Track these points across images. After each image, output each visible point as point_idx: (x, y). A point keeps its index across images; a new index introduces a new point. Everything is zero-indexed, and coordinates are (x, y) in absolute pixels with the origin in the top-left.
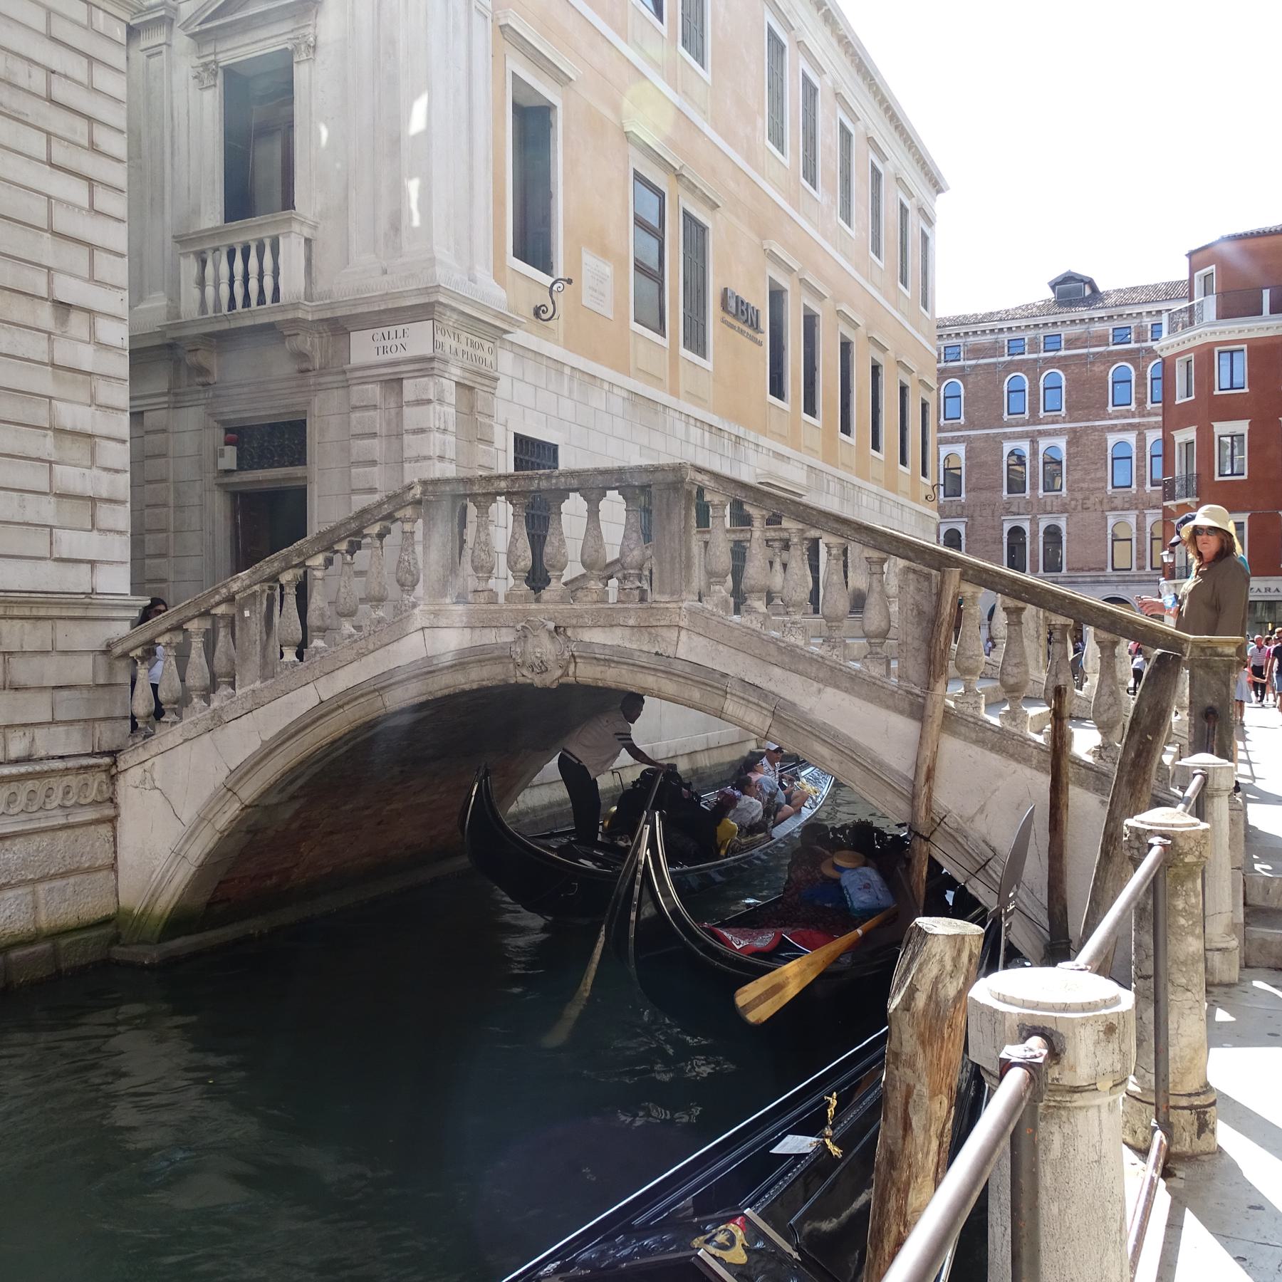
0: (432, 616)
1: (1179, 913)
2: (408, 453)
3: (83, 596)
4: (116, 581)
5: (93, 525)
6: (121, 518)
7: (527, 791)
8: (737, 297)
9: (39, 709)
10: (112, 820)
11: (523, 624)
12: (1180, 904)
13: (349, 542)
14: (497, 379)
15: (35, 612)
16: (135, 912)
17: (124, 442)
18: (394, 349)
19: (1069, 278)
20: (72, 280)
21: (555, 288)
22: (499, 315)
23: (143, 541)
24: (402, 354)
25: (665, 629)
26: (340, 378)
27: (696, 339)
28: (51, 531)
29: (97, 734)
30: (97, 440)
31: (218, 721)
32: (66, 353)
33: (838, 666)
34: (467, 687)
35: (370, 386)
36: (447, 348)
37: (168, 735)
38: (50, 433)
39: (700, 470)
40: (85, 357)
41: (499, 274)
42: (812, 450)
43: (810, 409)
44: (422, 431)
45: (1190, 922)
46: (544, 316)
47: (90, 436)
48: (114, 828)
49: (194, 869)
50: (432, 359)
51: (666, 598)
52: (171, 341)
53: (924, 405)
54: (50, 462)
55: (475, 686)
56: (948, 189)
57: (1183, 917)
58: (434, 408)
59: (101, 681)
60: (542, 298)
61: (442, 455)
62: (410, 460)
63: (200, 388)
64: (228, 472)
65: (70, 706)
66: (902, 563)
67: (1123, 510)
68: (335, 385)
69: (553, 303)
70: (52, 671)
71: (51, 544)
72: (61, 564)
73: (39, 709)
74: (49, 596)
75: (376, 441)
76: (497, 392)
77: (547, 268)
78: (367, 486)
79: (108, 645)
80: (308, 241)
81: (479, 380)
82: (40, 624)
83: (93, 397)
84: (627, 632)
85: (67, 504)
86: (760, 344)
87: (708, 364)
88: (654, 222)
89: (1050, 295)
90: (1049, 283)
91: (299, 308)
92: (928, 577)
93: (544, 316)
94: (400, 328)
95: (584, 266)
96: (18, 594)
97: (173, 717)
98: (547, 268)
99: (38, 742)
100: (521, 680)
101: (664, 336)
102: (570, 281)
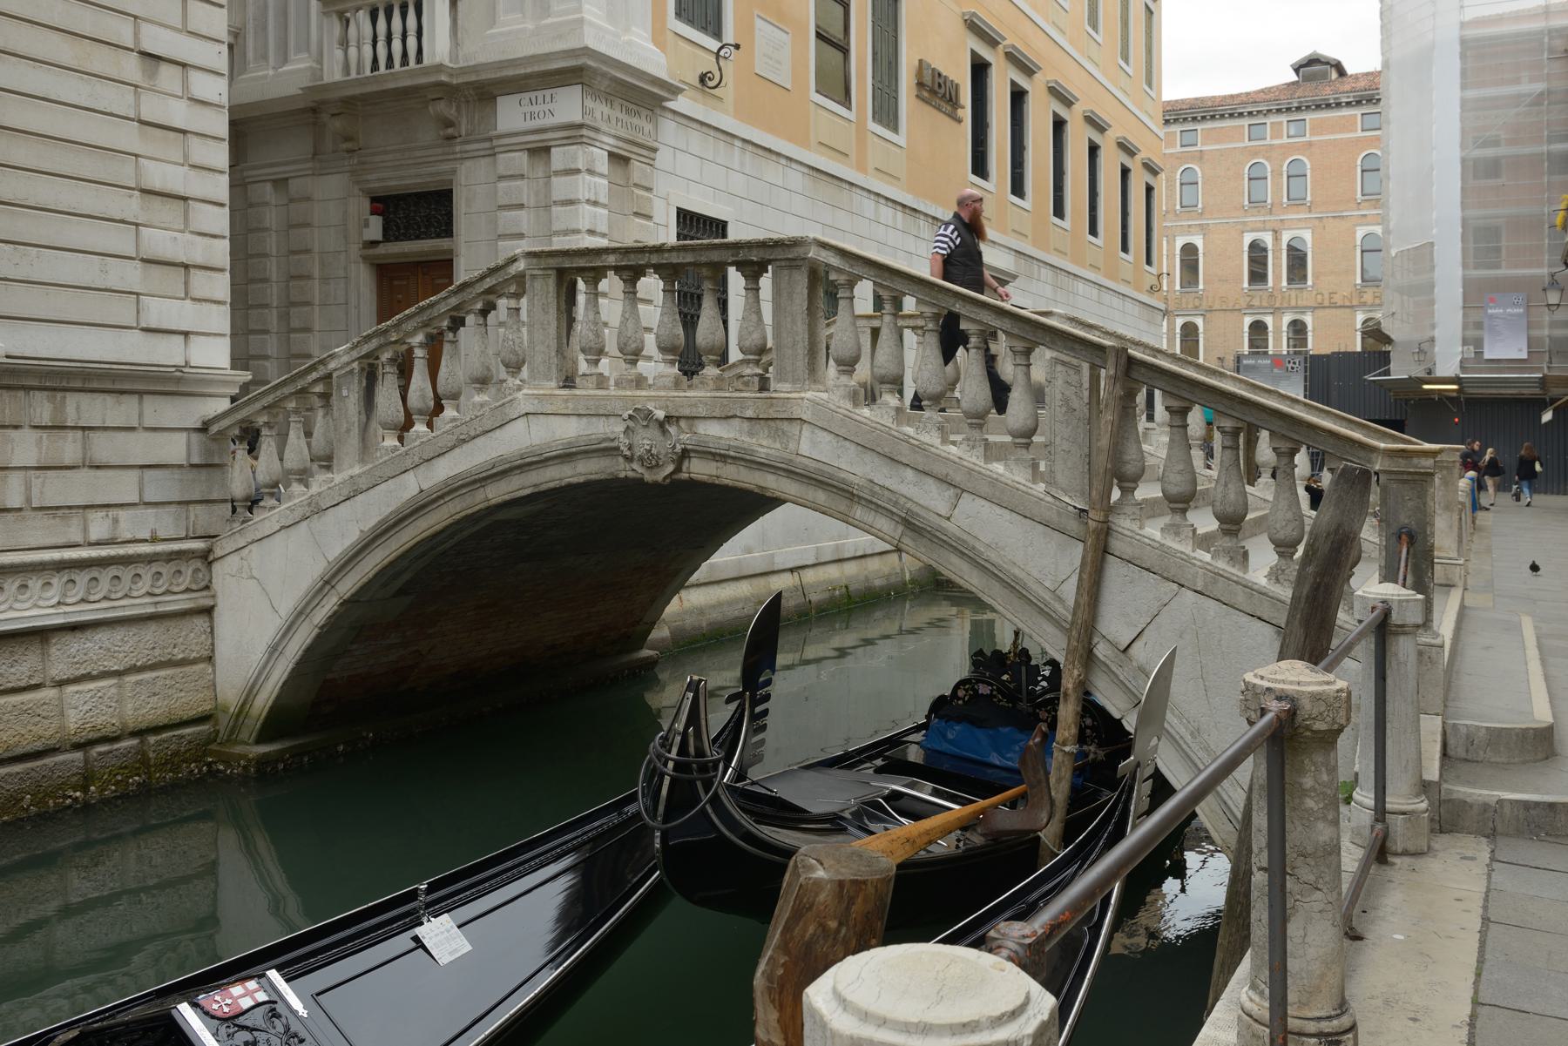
0: (536, 401)
1: (1304, 793)
3: (173, 369)
4: (214, 355)
5: (186, 293)
6: (220, 286)
7: (683, 593)
8: (934, 70)
9: (124, 487)
10: (208, 611)
11: (631, 412)
12: (1308, 782)
13: (451, 317)
14: (655, 150)
15: (118, 386)
17: (222, 205)
18: (542, 115)
19: (1313, 61)
20: (162, 30)
21: (722, 53)
22: (656, 81)
23: (289, 314)
24: (549, 121)
25: (786, 423)
26: (487, 145)
27: (887, 112)
28: (138, 298)
29: (192, 518)
30: (190, 202)
31: (316, 510)
32: (152, 108)
33: (977, 468)
34: (574, 480)
35: (517, 154)
36: (598, 115)
38: (137, 193)
39: (824, 246)
40: (178, 113)
41: (658, 37)
42: (1021, 234)
43: (1018, 188)
44: (571, 202)
45: (1321, 806)
46: (711, 84)
47: (185, 199)
49: (291, 666)
50: (581, 126)
52: (315, 104)
54: (137, 225)
55: (581, 479)
57: (1312, 798)
58: (584, 179)
59: (196, 460)
60: (709, 64)
61: (592, 228)
63: (346, 155)
64: (374, 243)
65: (160, 487)
66: (1049, 354)
68: (482, 153)
69: (720, 69)
70: (140, 448)
71: (138, 312)
72: (150, 334)
73: (124, 487)
74: (162, 369)
75: (523, 213)
76: (657, 164)
77: (717, 34)
81: (635, 149)
82: (125, 398)
83: (186, 156)
84: (746, 425)
85: (156, 271)
86: (959, 121)
87: (900, 139)
89: (1293, 77)
91: (441, 71)
92: (1077, 369)
93: (711, 84)
94: (548, 93)
95: (757, 32)
96: (79, 365)
97: (273, 502)
98: (717, 34)
99: (123, 525)
100: (631, 474)
101: (849, 108)
102: (737, 47)
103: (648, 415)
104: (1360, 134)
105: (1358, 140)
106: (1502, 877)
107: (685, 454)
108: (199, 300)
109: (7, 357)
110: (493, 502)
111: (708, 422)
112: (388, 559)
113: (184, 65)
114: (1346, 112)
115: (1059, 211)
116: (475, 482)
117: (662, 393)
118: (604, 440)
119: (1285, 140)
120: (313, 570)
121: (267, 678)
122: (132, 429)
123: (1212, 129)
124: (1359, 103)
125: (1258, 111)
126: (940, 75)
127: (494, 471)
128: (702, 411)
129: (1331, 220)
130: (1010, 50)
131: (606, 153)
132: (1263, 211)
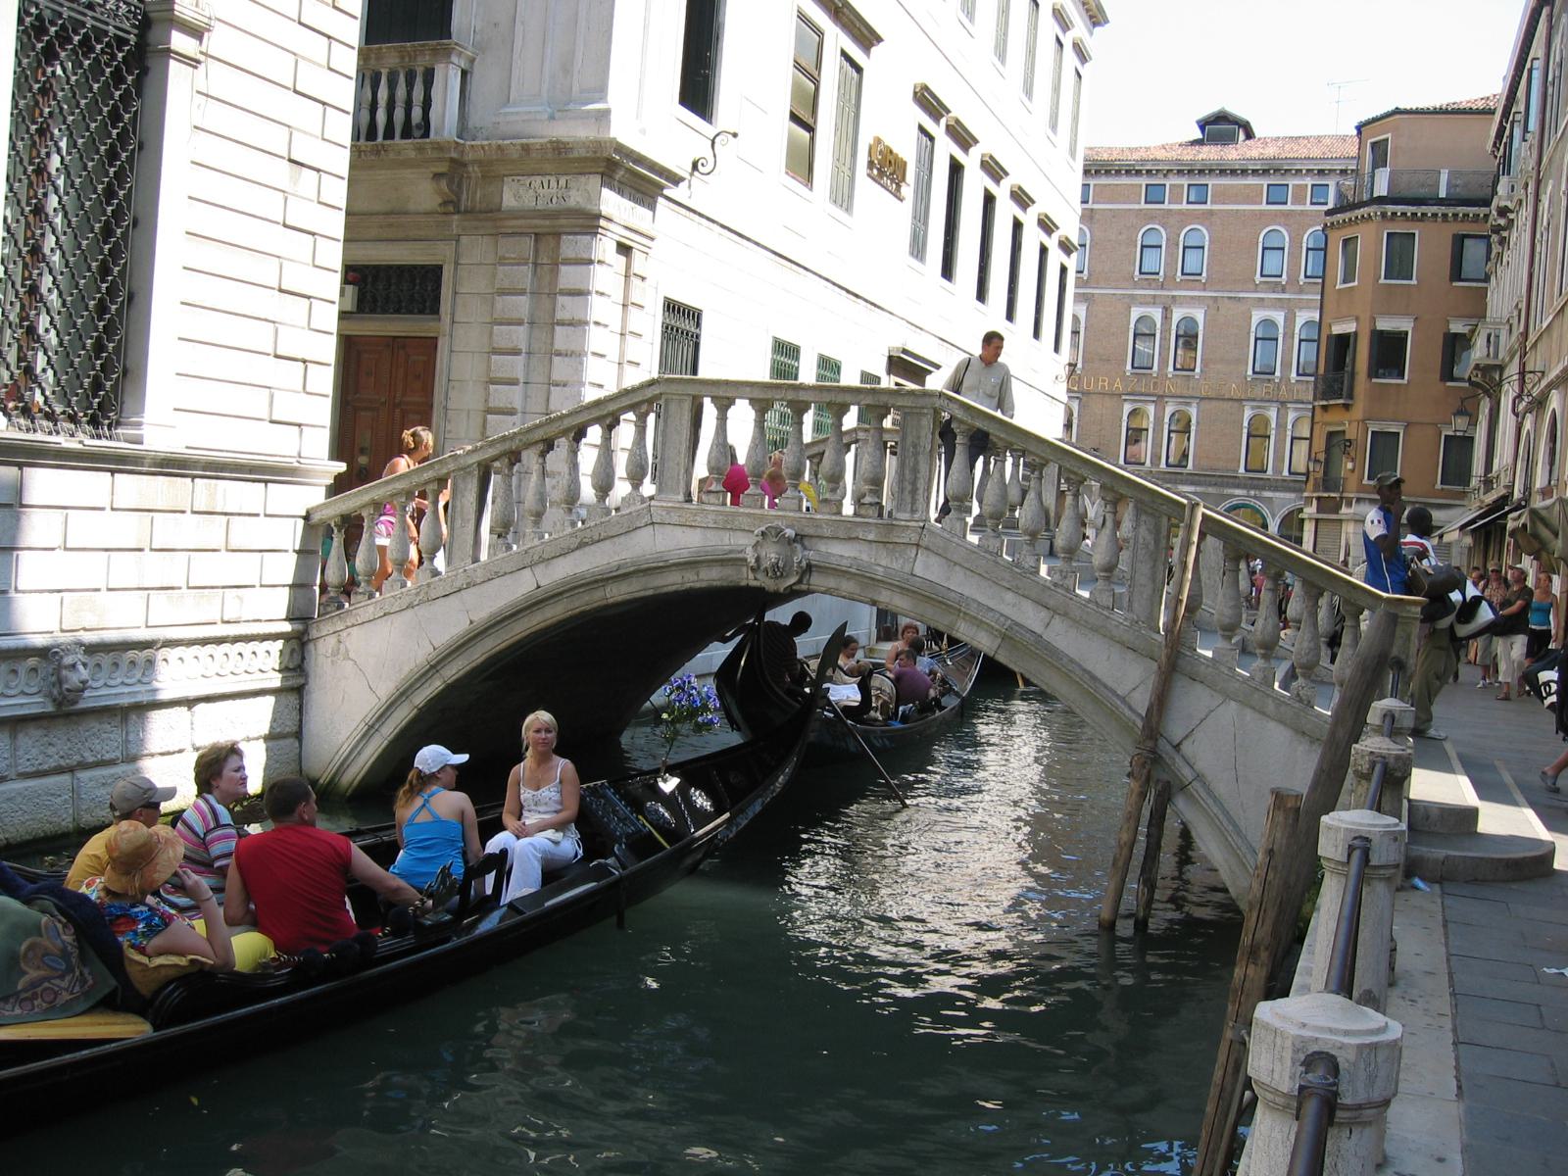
2: (560, 315)
16: (321, 781)
22: (653, 167)
27: (843, 198)
34: (698, 585)
37: (361, 607)
48: (301, 698)
51: (907, 516)
53: (1063, 270)
55: (704, 585)
56: (1107, 21)
62: (562, 323)
67: (1262, 400)
75: (523, 298)
78: (510, 345)
79: (308, 512)
80: (464, 73)
88: (812, 69)
90: (1198, 122)
102: (735, 135)
103: (779, 532)
104: (1264, 207)
105: (1262, 213)
106: (1448, 901)
107: (810, 567)
108: (311, 394)
109: (187, 447)
110: (611, 601)
111: (829, 542)
112: (498, 648)
113: (318, 171)
114: (1251, 181)
115: (1037, 334)
116: (596, 581)
117: (792, 514)
118: (731, 552)
119: (1184, 206)
120: (420, 654)
121: (359, 753)
122: (257, 515)
123: (1105, 185)
124: (1266, 172)
125: (1157, 170)
126: (891, 152)
127: (619, 572)
128: (827, 532)
129: (1226, 300)
130: (987, 159)
131: (615, 244)
132: (1153, 285)
